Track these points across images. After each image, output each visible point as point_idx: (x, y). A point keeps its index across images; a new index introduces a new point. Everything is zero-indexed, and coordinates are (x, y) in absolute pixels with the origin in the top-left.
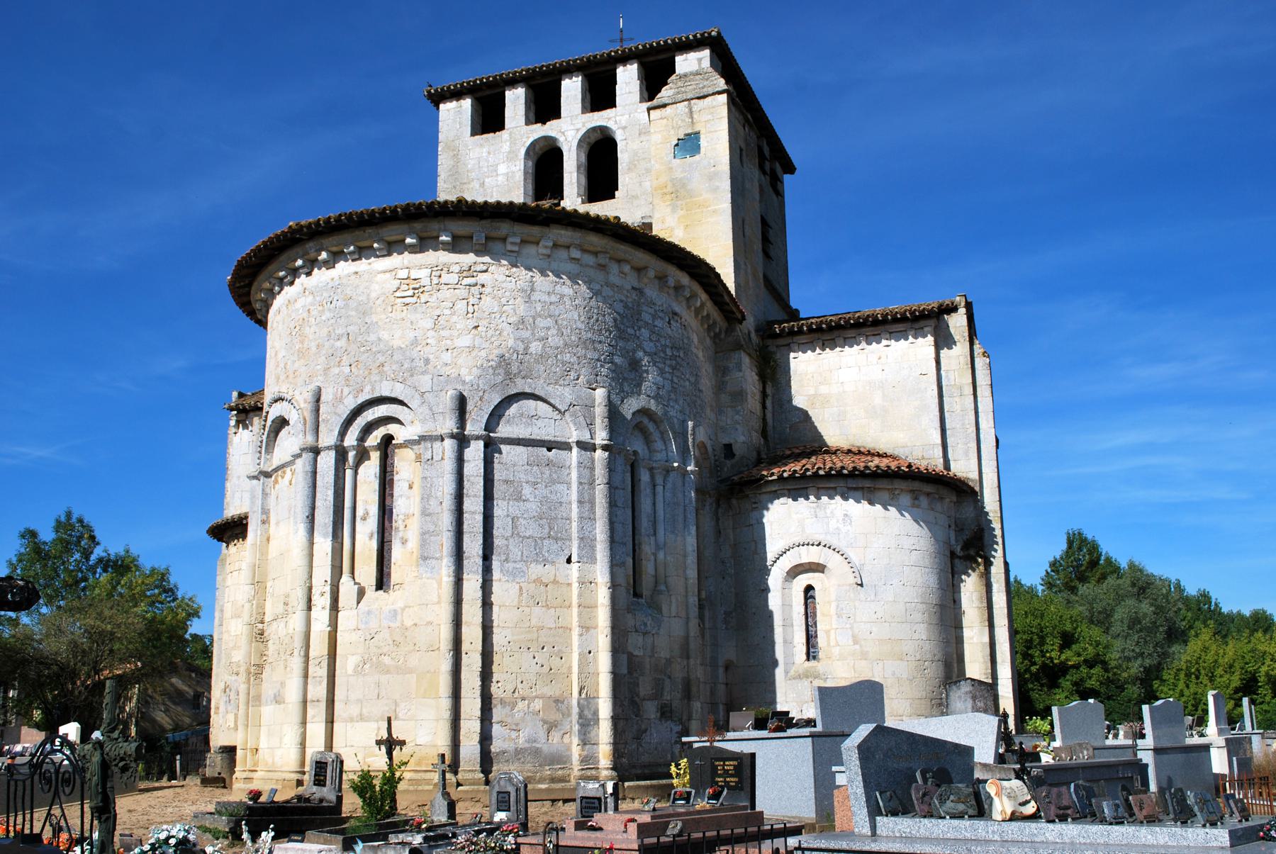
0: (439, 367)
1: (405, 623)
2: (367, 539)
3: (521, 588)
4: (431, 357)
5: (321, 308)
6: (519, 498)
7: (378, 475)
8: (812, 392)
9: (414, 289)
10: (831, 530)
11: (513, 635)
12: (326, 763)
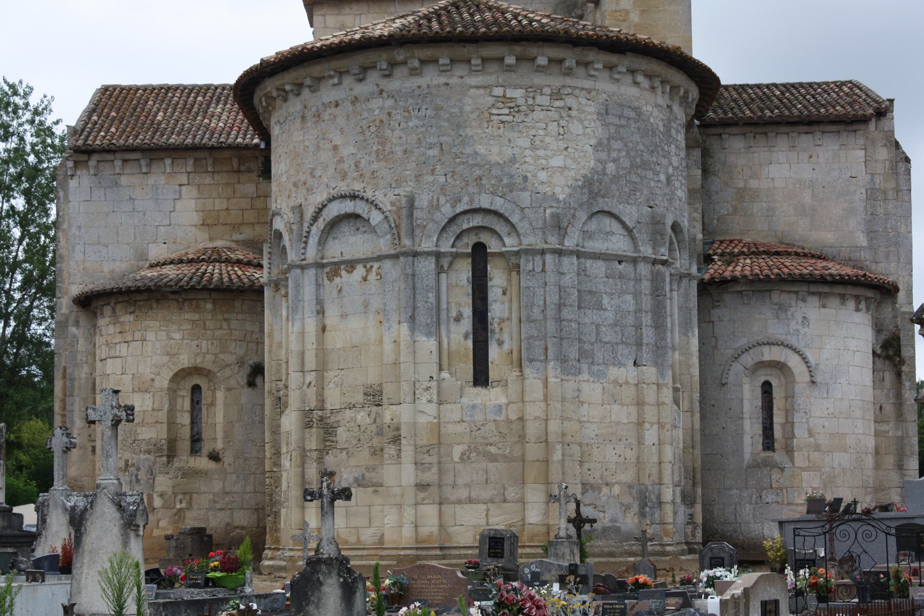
0: (536, 185)
1: (510, 417)
2: (462, 339)
3: (604, 387)
4: (529, 175)
5: (406, 114)
6: (601, 308)
7: (471, 279)
8: (741, 185)
9: (510, 108)
10: (791, 331)
11: (598, 429)
12: (503, 539)
